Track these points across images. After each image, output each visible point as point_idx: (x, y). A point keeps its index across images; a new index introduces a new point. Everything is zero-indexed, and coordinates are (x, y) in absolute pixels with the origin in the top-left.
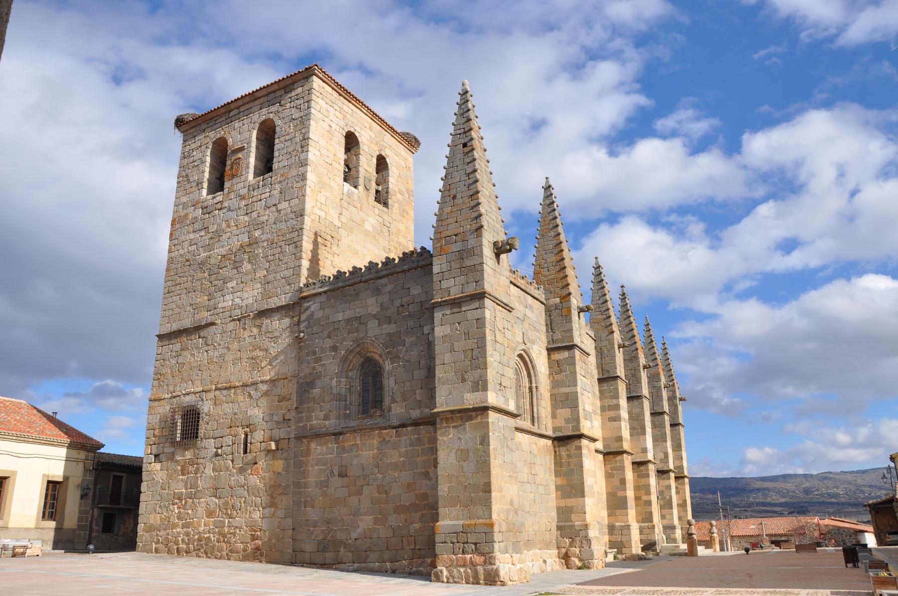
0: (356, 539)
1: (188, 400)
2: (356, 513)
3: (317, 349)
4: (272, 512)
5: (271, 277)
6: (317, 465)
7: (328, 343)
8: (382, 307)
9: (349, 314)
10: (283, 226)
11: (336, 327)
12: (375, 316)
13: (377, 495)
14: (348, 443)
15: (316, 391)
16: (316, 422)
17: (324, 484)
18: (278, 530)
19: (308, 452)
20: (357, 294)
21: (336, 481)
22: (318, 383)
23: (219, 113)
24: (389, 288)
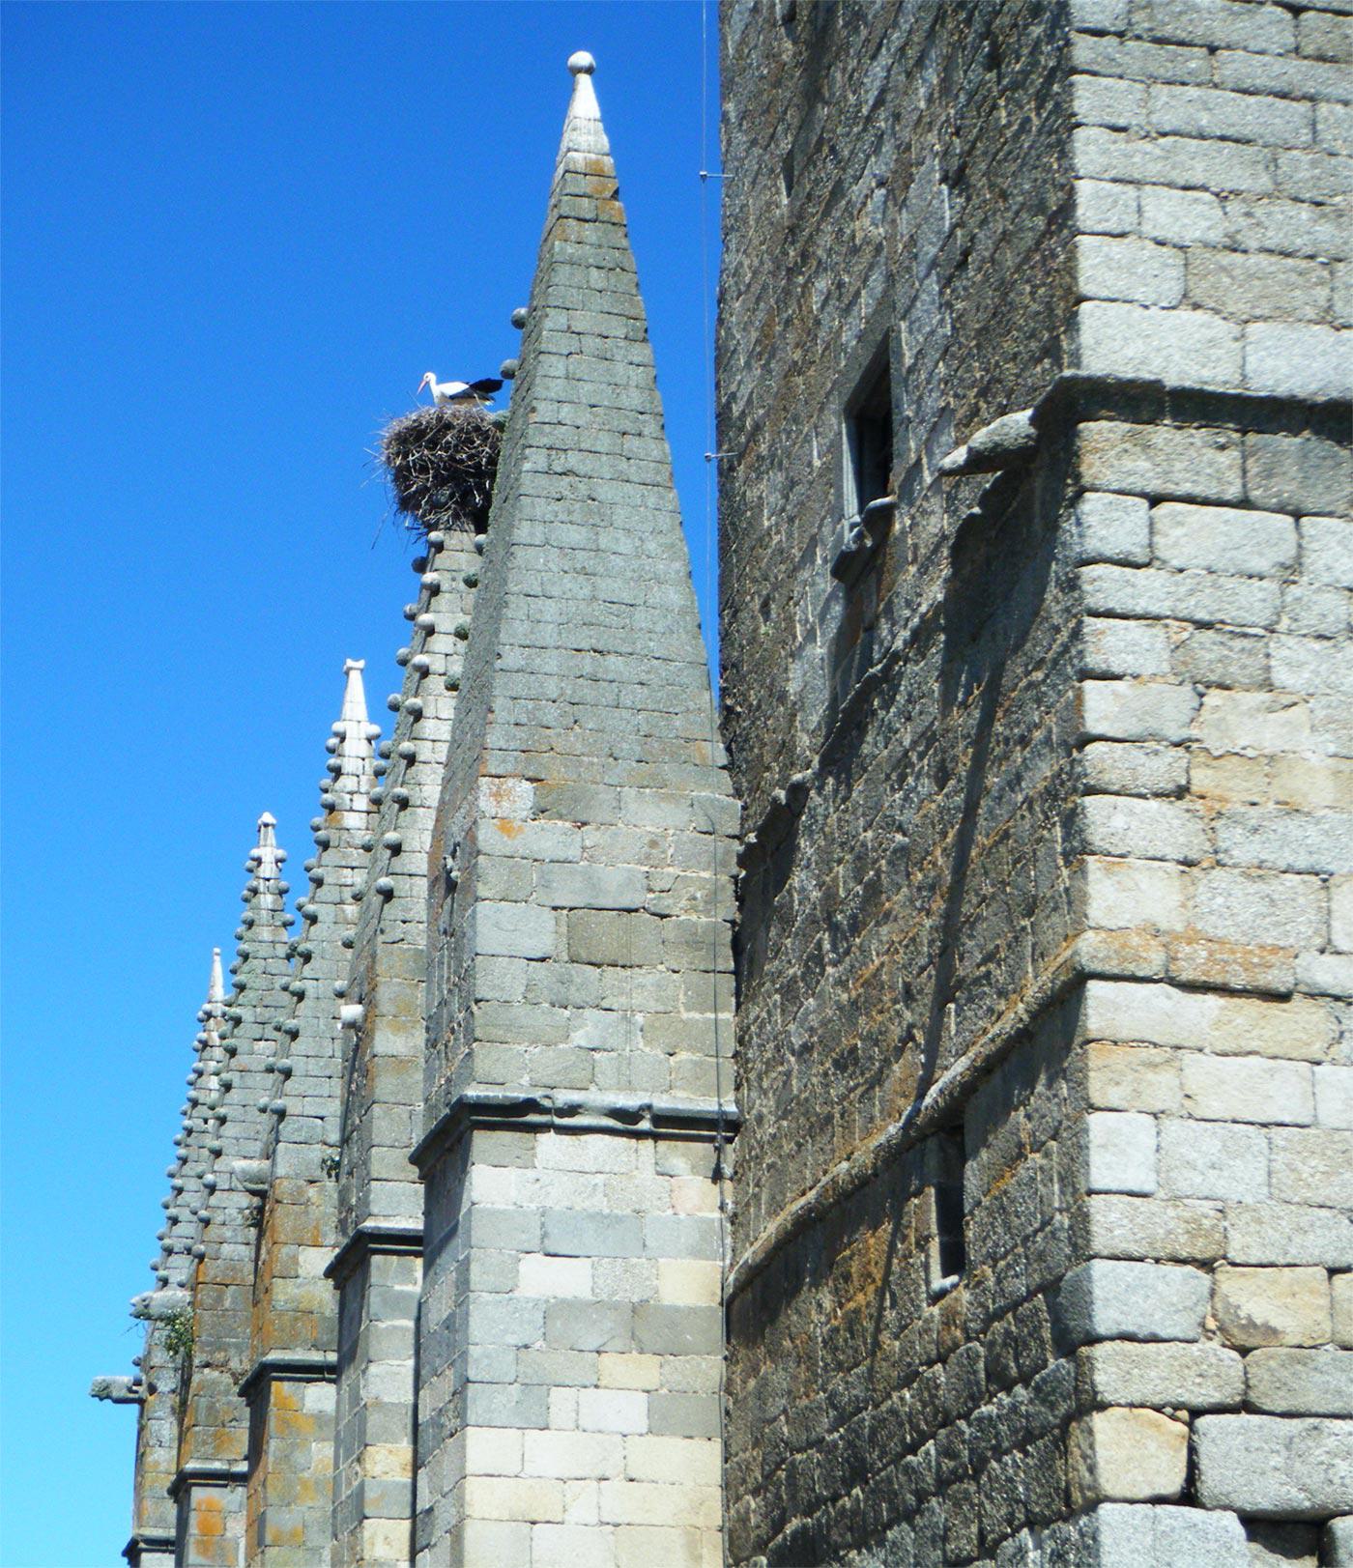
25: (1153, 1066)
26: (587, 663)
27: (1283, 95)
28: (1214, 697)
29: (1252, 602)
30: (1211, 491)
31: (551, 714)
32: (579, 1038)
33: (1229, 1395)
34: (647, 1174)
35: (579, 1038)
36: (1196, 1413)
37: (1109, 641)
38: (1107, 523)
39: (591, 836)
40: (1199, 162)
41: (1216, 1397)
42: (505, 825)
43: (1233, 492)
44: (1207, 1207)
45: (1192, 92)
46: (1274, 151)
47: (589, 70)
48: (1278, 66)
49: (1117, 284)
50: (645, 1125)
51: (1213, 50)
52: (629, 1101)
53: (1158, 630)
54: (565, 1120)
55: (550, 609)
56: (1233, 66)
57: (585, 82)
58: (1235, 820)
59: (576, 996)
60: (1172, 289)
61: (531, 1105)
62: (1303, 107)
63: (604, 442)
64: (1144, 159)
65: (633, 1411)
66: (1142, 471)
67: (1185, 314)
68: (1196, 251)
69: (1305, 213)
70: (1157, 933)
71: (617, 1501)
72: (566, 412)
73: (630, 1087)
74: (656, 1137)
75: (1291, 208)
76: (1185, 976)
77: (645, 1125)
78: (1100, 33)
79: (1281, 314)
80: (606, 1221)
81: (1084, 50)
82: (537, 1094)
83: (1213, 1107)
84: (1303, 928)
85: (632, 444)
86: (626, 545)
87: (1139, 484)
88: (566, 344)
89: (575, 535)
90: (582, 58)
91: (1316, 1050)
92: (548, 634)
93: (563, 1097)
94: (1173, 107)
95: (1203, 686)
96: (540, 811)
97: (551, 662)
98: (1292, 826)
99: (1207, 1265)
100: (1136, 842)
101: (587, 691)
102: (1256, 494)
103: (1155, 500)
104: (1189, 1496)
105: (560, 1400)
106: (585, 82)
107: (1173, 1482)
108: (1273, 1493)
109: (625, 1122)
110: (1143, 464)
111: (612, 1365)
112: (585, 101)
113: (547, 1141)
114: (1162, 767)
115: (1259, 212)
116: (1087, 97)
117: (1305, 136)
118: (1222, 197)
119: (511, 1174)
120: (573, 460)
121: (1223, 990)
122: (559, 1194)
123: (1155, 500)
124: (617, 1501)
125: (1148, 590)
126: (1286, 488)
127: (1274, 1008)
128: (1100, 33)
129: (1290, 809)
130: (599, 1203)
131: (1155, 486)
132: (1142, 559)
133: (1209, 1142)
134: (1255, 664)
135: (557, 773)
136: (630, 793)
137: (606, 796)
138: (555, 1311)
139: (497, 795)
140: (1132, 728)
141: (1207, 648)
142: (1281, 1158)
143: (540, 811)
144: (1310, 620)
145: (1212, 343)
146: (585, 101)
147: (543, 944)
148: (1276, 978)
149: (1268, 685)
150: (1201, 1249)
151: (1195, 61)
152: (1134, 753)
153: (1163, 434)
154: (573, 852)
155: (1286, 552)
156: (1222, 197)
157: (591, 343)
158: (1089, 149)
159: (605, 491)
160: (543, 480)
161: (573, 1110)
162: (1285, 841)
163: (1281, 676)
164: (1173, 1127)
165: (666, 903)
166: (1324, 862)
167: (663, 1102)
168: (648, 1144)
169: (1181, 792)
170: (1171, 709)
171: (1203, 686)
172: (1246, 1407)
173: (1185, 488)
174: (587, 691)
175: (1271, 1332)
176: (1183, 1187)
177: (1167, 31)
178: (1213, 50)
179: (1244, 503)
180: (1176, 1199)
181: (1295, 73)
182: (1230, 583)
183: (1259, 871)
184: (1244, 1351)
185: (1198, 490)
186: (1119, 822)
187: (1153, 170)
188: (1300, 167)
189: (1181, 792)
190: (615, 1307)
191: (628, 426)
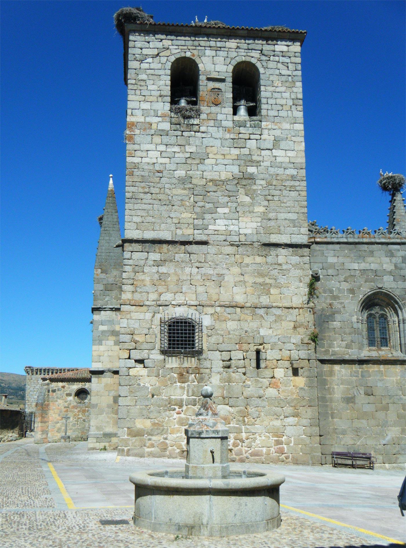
0: (384, 445)
1: (180, 312)
2: (384, 425)
3: (334, 289)
4: (296, 421)
5: (272, 215)
6: (342, 384)
7: (345, 286)
8: (396, 266)
9: (363, 266)
10: (280, 171)
11: (352, 274)
12: (390, 273)
13: (403, 411)
14: (372, 370)
15: (336, 324)
16: (338, 349)
17: (350, 400)
18: (304, 436)
19: (331, 373)
20: (372, 252)
21: (361, 398)
22: (338, 317)
23: (184, 31)
24: (402, 253)
25: (127, 314)
26: (108, 254)
27: (150, 204)
28: (137, 274)
29: (142, 263)
30: (138, 250)
31: (103, 261)
32: (106, 300)
33: (134, 348)
34: (114, 315)
35: (106, 300)
36: (130, 350)
37: (126, 268)
38: (126, 255)
39: (108, 275)
40: (139, 213)
41: (132, 348)
42: (97, 275)
43: (141, 250)
44: (133, 329)
45: (139, 205)
46: (148, 211)
47: (112, 177)
48: (149, 201)
49: (129, 228)
50: (114, 310)
51: (142, 199)
52: (111, 307)
53: (131, 267)
54: (104, 309)
55: (104, 248)
56: (144, 201)
57: (111, 179)
58: (138, 287)
59: (105, 294)
60: (135, 228)
61: (100, 308)
62: (152, 205)
63: (111, 226)
64: (133, 213)
65: (112, 343)
66: (131, 249)
67: (137, 231)
68: (138, 223)
69: (151, 218)
70: (129, 300)
71: (110, 353)
72: (107, 222)
73: (112, 305)
74: (115, 311)
75: (149, 217)
76: (132, 304)
77: (114, 310)
78: (129, 199)
79: (148, 230)
80: (109, 321)
81: (127, 201)
82: (101, 307)
83: (134, 318)
84: (145, 298)
85: (115, 226)
86: (113, 239)
87: (130, 250)
88: (107, 213)
89: (107, 238)
90: (111, 175)
91: (146, 311)
92: (103, 251)
93: (104, 307)
94: (137, 207)
95: (136, 272)
96: (102, 273)
97: (103, 254)
98: (145, 287)
99: (132, 335)
100: (127, 290)
101: (108, 258)
102: (143, 250)
103: (132, 252)
104: (129, 358)
105: (103, 342)
106: (111, 179)
107: (127, 357)
108: (138, 357)
109: (111, 309)
110: (131, 248)
111: (110, 337)
112: (111, 181)
113: (102, 312)
114: (131, 282)
115: (146, 218)
116: (127, 206)
117: (152, 209)
118: (142, 217)
119: (98, 316)
120: (107, 229)
121: (135, 306)
122: (104, 318)
123: (132, 252)
124: (110, 353)
125: (131, 262)
126: (147, 250)
127: (141, 307)
128: (129, 199)
129: (145, 286)
130: (108, 319)
131: (132, 250)
132: (130, 258)
133: (133, 322)
134: (142, 270)
135: (104, 268)
136: (112, 270)
137: (109, 270)
138: (103, 332)
139: (96, 271)
140: (127, 277)
141: (137, 268)
142: (141, 323)
143: (102, 273)
144: (148, 264)
145: (140, 234)
146: (111, 181)
147: (102, 289)
148: (142, 304)
149: (143, 272)
150: (132, 333)
151: (139, 201)
152: (128, 280)
153: (133, 245)
154: (106, 277)
155: (147, 257)
156: (142, 217)
157: (110, 213)
158: (127, 212)
159: (111, 232)
160: (103, 231)
161: (105, 308)
162: (144, 289)
163: (145, 271)
164: (129, 320)
165: (117, 283)
166: (148, 291)
167: (116, 307)
168: (114, 312)
169: (133, 284)
170: (132, 275)
171: (136, 272)
172: (135, 349)
173: (135, 250)
174: (108, 258)
175: (138, 341)
176: (130, 326)
177: (137, 198)
178: (142, 199)
179: (142, 252)
180: (129, 328)
181: (151, 201)
182: (139, 261)
183: (141, 292)
184: (136, 343)
185: (137, 251)
186: (125, 288)
187: (134, 214)
188: (151, 213)
189: (133, 284)
190: (110, 331)
191: (114, 223)
